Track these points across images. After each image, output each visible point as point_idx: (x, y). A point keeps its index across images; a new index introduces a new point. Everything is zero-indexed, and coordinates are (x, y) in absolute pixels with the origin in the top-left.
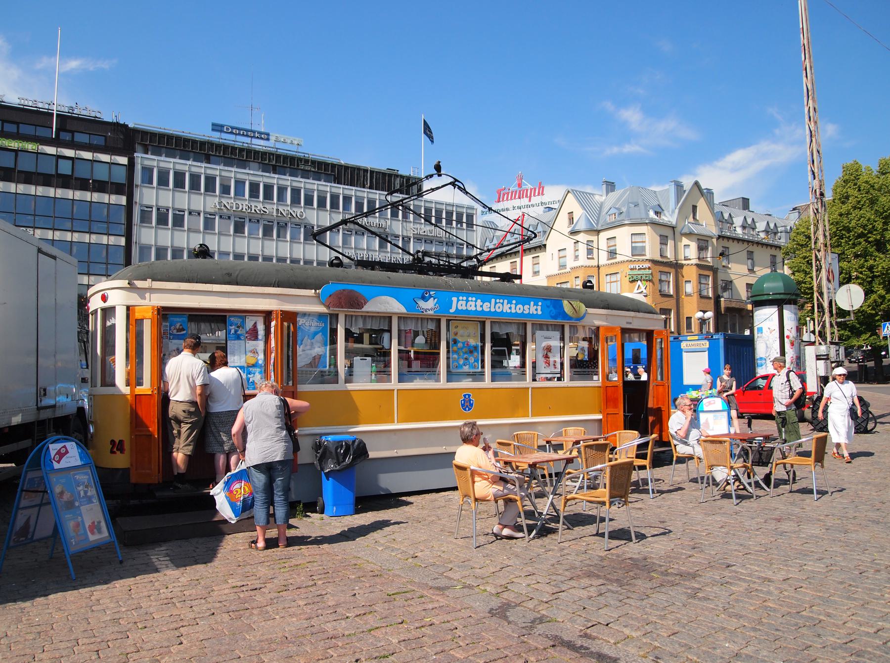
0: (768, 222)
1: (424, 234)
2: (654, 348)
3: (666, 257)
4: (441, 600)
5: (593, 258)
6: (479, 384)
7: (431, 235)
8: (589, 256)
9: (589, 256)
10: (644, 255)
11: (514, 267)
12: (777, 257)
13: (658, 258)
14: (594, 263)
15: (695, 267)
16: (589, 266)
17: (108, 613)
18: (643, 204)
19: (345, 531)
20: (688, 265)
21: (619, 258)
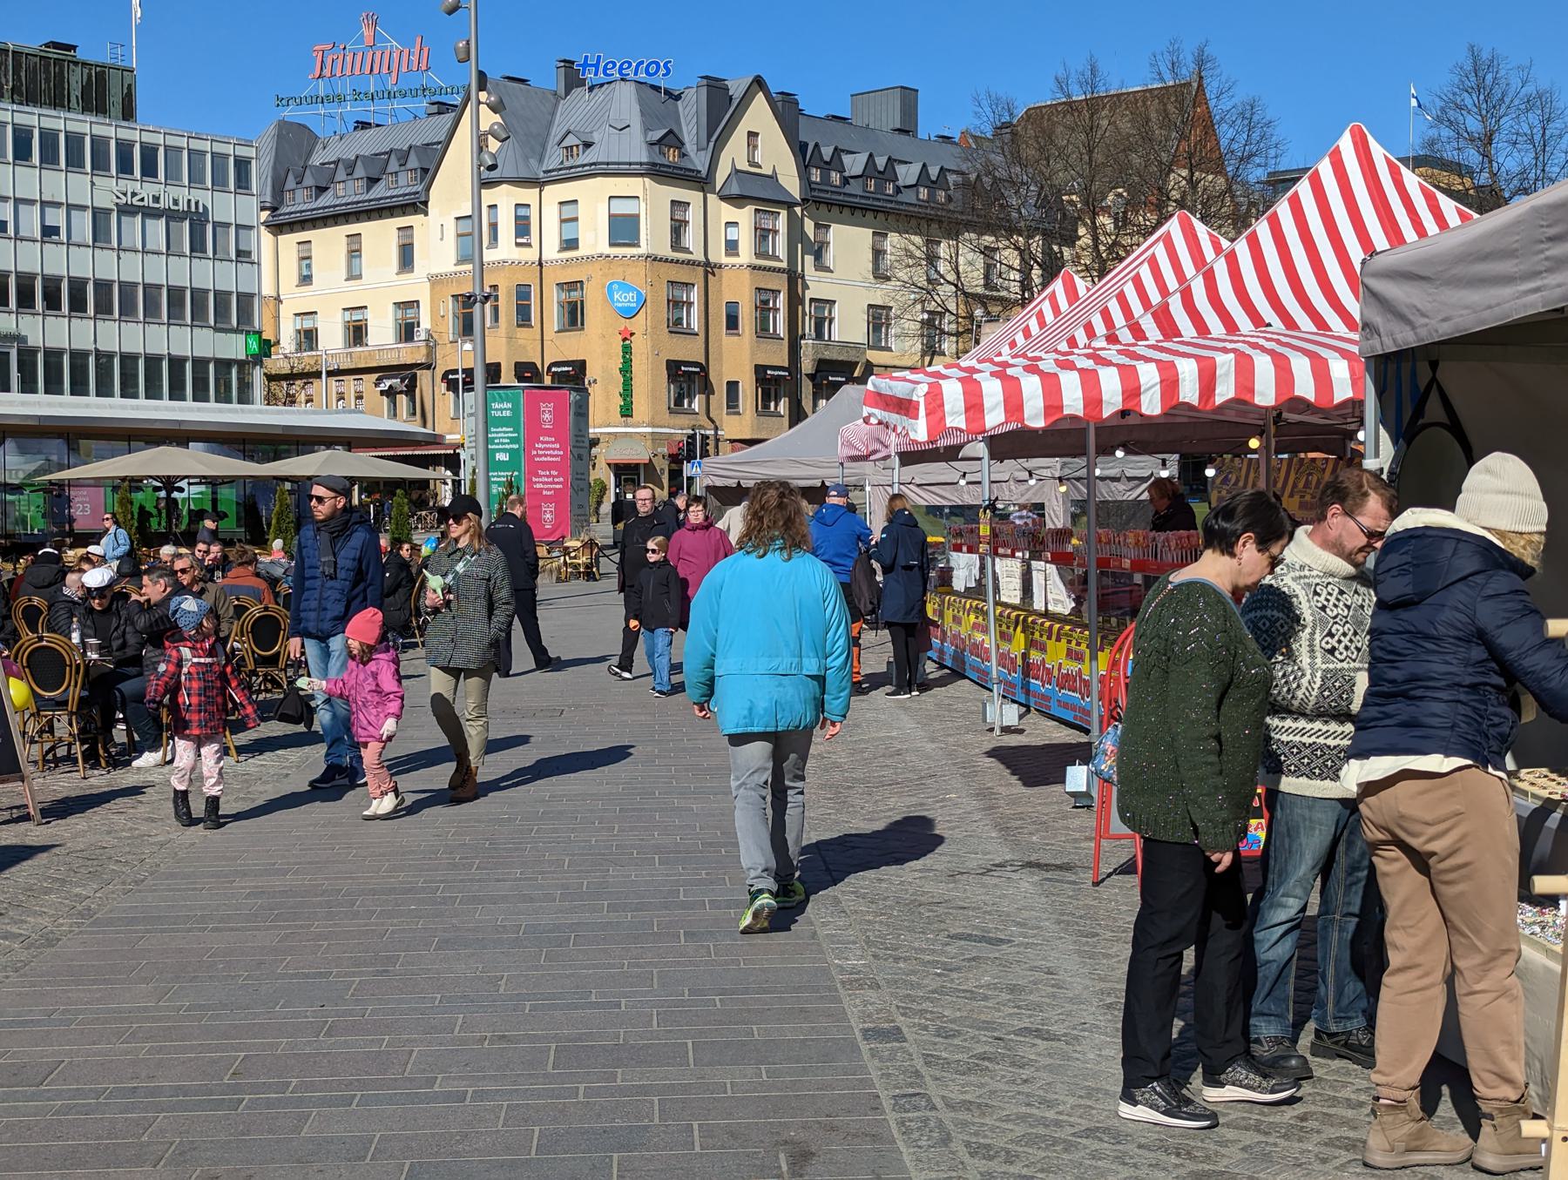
0: (871, 155)
1: (141, 204)
2: (183, 427)
3: (687, 251)
4: (1016, 1128)
5: (529, 245)
6: (745, 396)
7: (157, 205)
8: (519, 240)
9: (519, 240)
10: (637, 245)
11: (356, 247)
12: (416, 232)
13: (667, 252)
14: (530, 255)
15: (747, 272)
16: (661, 260)
17: (456, 530)
18: (1207, 237)
19: (1128, 452)
20: (677, 261)
21: (583, 251)
